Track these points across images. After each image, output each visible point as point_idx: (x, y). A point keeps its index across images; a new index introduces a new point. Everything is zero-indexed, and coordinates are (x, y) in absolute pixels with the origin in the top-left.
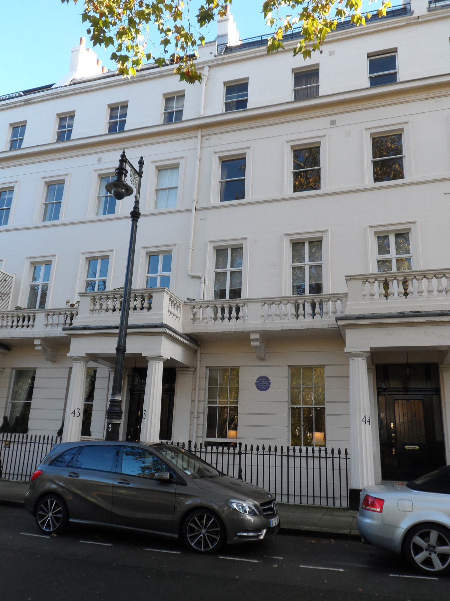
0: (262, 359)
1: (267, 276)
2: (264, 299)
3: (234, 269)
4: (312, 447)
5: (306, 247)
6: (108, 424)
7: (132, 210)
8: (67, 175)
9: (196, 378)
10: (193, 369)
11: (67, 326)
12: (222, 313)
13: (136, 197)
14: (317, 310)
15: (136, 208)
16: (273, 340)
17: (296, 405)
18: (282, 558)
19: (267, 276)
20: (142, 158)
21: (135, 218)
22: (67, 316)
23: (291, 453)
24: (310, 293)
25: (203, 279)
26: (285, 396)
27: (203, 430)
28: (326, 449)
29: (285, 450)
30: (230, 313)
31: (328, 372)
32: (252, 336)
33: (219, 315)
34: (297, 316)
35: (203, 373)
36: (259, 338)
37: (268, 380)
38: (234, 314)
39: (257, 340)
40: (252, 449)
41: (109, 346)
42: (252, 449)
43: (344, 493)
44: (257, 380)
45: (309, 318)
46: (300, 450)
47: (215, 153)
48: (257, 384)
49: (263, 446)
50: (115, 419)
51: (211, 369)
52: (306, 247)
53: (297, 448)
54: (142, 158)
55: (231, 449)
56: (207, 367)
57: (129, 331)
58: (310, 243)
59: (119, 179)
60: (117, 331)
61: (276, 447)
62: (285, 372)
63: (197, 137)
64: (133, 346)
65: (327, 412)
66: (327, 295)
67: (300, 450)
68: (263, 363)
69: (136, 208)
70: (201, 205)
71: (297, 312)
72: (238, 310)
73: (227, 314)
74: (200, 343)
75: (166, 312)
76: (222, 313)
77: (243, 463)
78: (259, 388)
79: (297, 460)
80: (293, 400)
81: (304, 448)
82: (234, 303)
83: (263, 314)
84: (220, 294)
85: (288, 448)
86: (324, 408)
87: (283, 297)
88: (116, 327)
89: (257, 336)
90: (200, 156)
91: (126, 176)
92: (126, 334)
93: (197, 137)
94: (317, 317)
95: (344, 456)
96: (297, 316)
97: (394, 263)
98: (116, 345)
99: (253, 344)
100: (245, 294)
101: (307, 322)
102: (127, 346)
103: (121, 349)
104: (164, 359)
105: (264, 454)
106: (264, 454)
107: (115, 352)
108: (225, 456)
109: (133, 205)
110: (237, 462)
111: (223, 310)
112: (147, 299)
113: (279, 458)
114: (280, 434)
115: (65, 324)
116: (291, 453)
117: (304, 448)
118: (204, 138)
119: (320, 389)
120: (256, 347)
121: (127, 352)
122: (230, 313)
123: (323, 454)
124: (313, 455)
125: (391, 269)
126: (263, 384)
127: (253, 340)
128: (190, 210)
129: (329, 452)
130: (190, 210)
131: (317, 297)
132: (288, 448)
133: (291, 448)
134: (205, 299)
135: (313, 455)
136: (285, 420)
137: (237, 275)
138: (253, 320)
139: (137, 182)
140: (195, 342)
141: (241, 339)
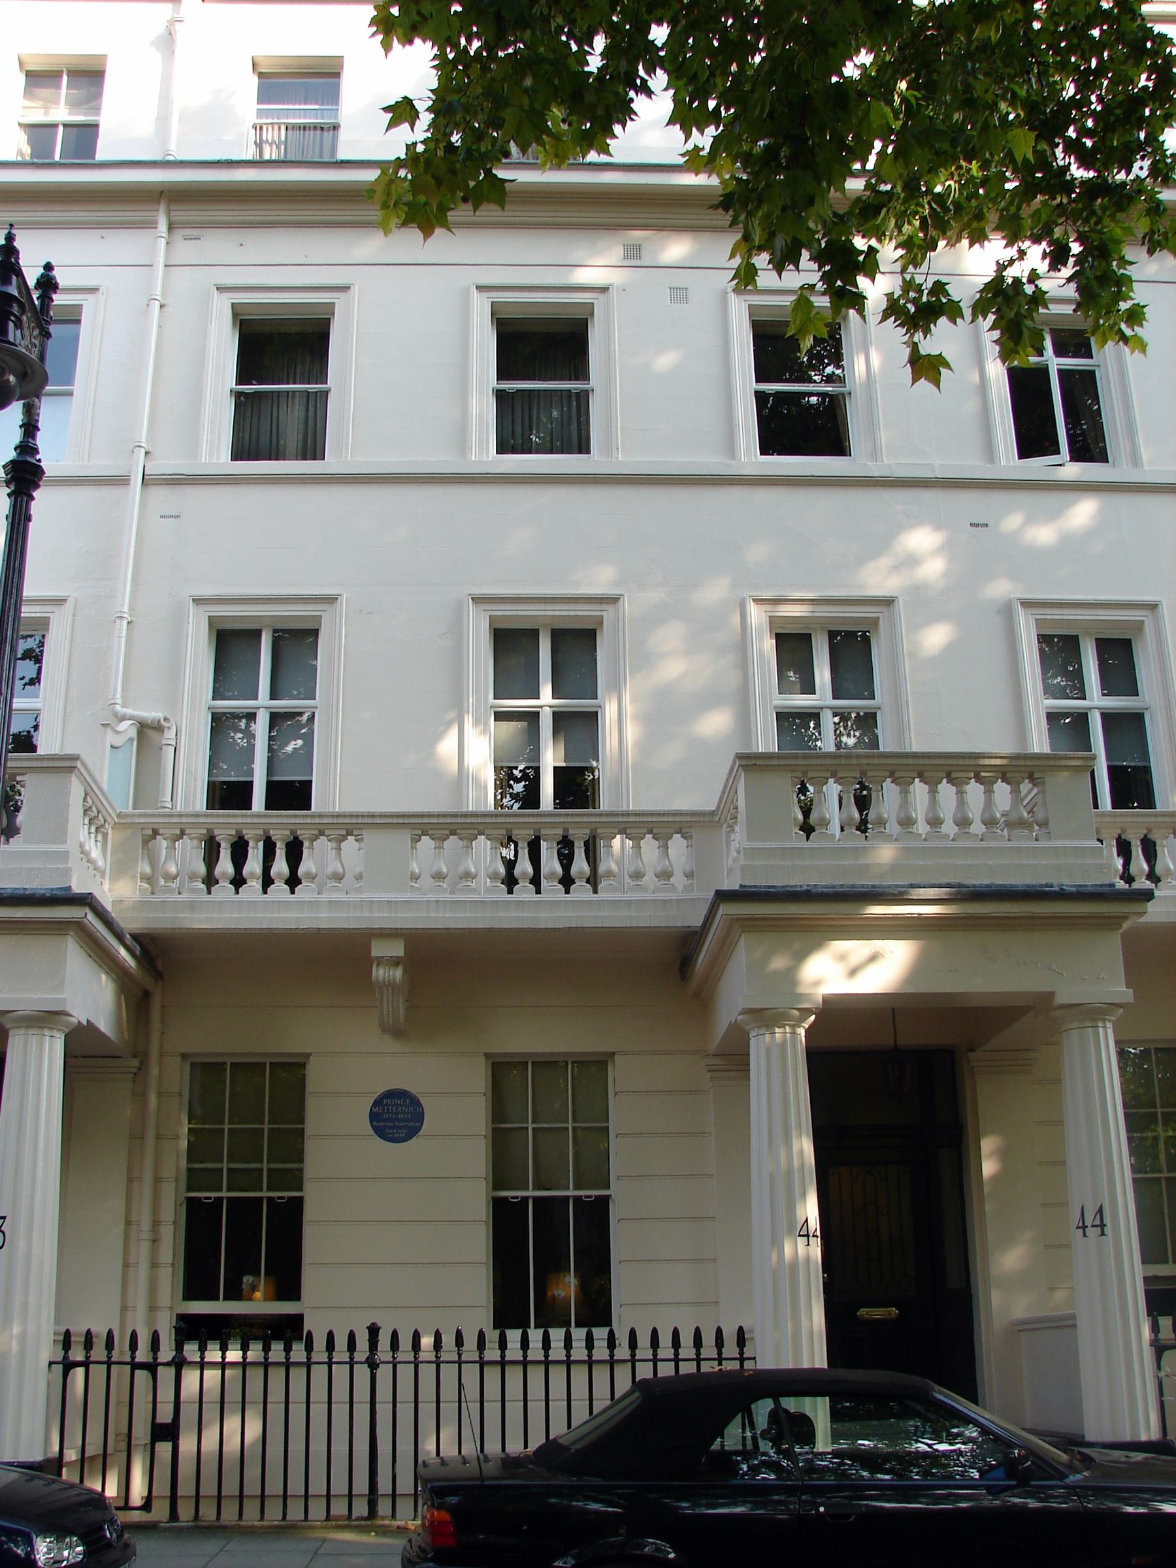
1: (419, 741)
2: (422, 816)
3: (282, 704)
4: (606, 1330)
5: (264, 650)
7: (12, 455)
8: (94, 290)
9: (144, 1096)
10: (135, 1063)
12: (224, 857)
14: (580, 865)
15: (27, 447)
19: (419, 741)
20: (48, 267)
23: (492, 1354)
24: (268, 806)
25: (170, 735)
26: (475, 1158)
27: (170, 1281)
29: (470, 1342)
30: (566, 860)
31: (619, 1075)
32: (379, 949)
33: (225, 866)
34: (210, 881)
35: (170, 1078)
36: (401, 953)
37: (415, 1102)
38: (280, 866)
39: (395, 962)
40: (633, 1344)
42: (633, 1344)
43: (406, 1484)
44: (375, 1104)
45: (552, 889)
46: (525, 1344)
47: (220, 289)
48: (373, 1117)
52: (264, 650)
53: (514, 1335)
54: (48, 267)
55: (277, 1348)
56: (184, 1056)
61: (655, 1332)
63: (153, 225)
65: (309, 1213)
66: (612, 814)
67: (525, 1344)
69: (27, 447)
70: (164, 465)
71: (566, 867)
72: (295, 852)
73: (253, 864)
74: (160, 966)
76: (224, 857)
78: (381, 1132)
79: (514, 1376)
80: (502, 1171)
81: (579, 1334)
82: (284, 822)
84: (229, 795)
85: (481, 1336)
86: (606, 1199)
87: (465, 815)
90: (163, 294)
93: (153, 225)
94: (581, 891)
95: (670, 1353)
96: (210, 881)
97: (263, 720)
99: (380, 973)
100: (326, 797)
101: (549, 908)
104: (71, 1023)
105: (460, 1363)
106: (460, 1363)
108: (277, 1377)
109: (16, 436)
111: (239, 852)
113: (341, 1373)
114: (459, 1287)
116: (492, 1354)
117: (536, 1335)
118: (179, 233)
119: (595, 1137)
122: (566, 860)
123: (601, 1351)
124: (590, 1356)
126: (396, 1116)
127: (380, 961)
128: (121, 481)
129: (623, 1339)
130: (121, 481)
131: (577, 821)
132: (481, 1336)
133: (492, 1336)
134: (179, 809)
135: (568, 1355)
136: (476, 1244)
137: (578, 726)
138: (340, 891)
140: (158, 965)
141: (332, 961)
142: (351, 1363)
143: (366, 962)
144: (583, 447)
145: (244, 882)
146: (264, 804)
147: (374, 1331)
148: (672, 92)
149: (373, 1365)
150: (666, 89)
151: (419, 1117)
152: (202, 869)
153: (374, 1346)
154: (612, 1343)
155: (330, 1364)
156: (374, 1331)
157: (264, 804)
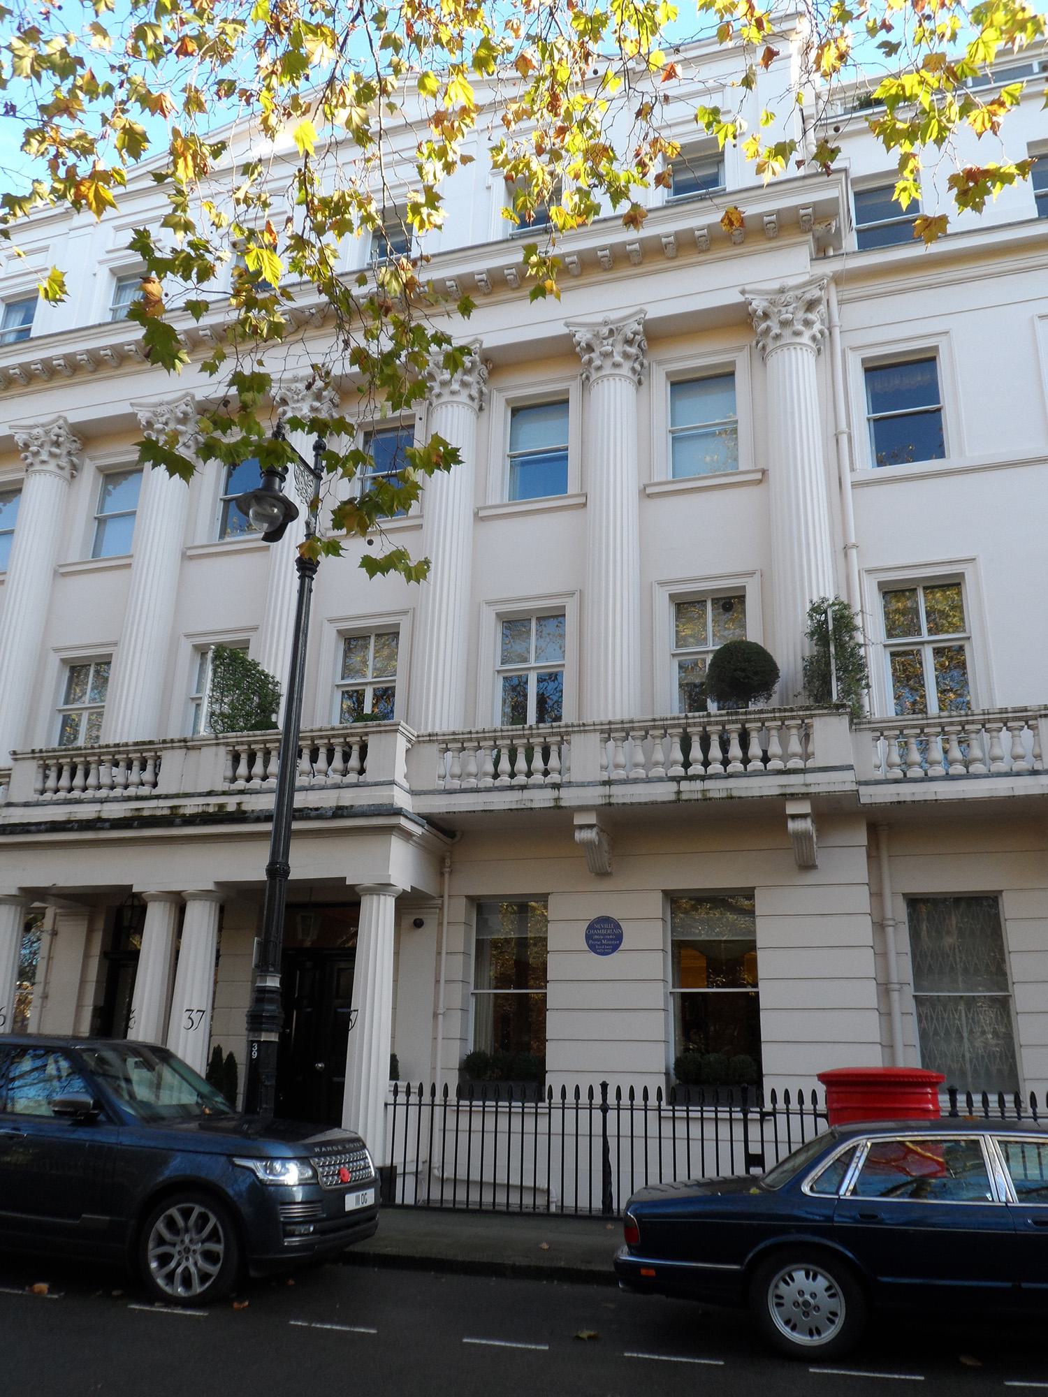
0: (603, 874)
6: (251, 1044)
11: (505, 780)
13: (308, 524)
16: (630, 829)
17: (527, 988)
18: (373, 1331)
21: (308, 573)
22: (499, 752)
28: (408, 1087)
32: (579, 820)
40: (577, 1096)
41: (250, 865)
49: (645, 1089)
50: (267, 1031)
51: (480, 906)
57: (296, 825)
58: (538, 619)
59: (268, 486)
60: (268, 827)
61: (645, 1089)
62: (655, 905)
64: (309, 863)
68: (606, 885)
75: (400, 774)
77: (612, 1130)
83: (605, 762)
88: (267, 818)
89: (591, 819)
91: (283, 479)
92: (290, 834)
98: (266, 861)
102: (293, 861)
103: (278, 869)
106: (646, 1110)
107: (264, 877)
110: (597, 1129)
112: (350, 751)
115: (496, 776)
120: (588, 844)
121: (293, 876)
125: (680, 667)
126: (604, 936)
139: (311, 490)
141: (550, 827)
142: (433, 1105)
143: (571, 828)
144: (941, 454)
145: (691, 765)
146: (535, 707)
147: (604, 1086)
148: (955, 191)
149: (605, 1109)
150: (950, 189)
151: (619, 938)
152: (679, 756)
153: (604, 1100)
154: (1018, 1102)
155: (420, 1105)
156: (604, 1086)
157: (535, 707)
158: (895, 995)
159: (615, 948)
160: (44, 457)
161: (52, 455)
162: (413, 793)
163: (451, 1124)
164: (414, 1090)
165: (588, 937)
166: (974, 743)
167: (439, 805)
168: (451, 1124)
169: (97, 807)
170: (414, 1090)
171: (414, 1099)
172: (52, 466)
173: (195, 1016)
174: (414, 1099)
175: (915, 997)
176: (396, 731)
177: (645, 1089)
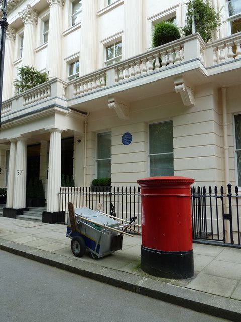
61: (134, 187)
147: (230, 186)
156: (230, 186)
158: (227, 151)
159: (130, 142)
160: (27, 18)
161: (29, 18)
162: (67, 101)
163: (88, 199)
164: (79, 189)
165: (122, 140)
166: (177, 54)
167: (74, 103)
168: (88, 199)
169: (8, 117)
170: (79, 189)
171: (79, 192)
172: (29, 21)
173: (19, 171)
174: (79, 192)
175: (237, 152)
176: (57, 81)
177: (134, 187)
